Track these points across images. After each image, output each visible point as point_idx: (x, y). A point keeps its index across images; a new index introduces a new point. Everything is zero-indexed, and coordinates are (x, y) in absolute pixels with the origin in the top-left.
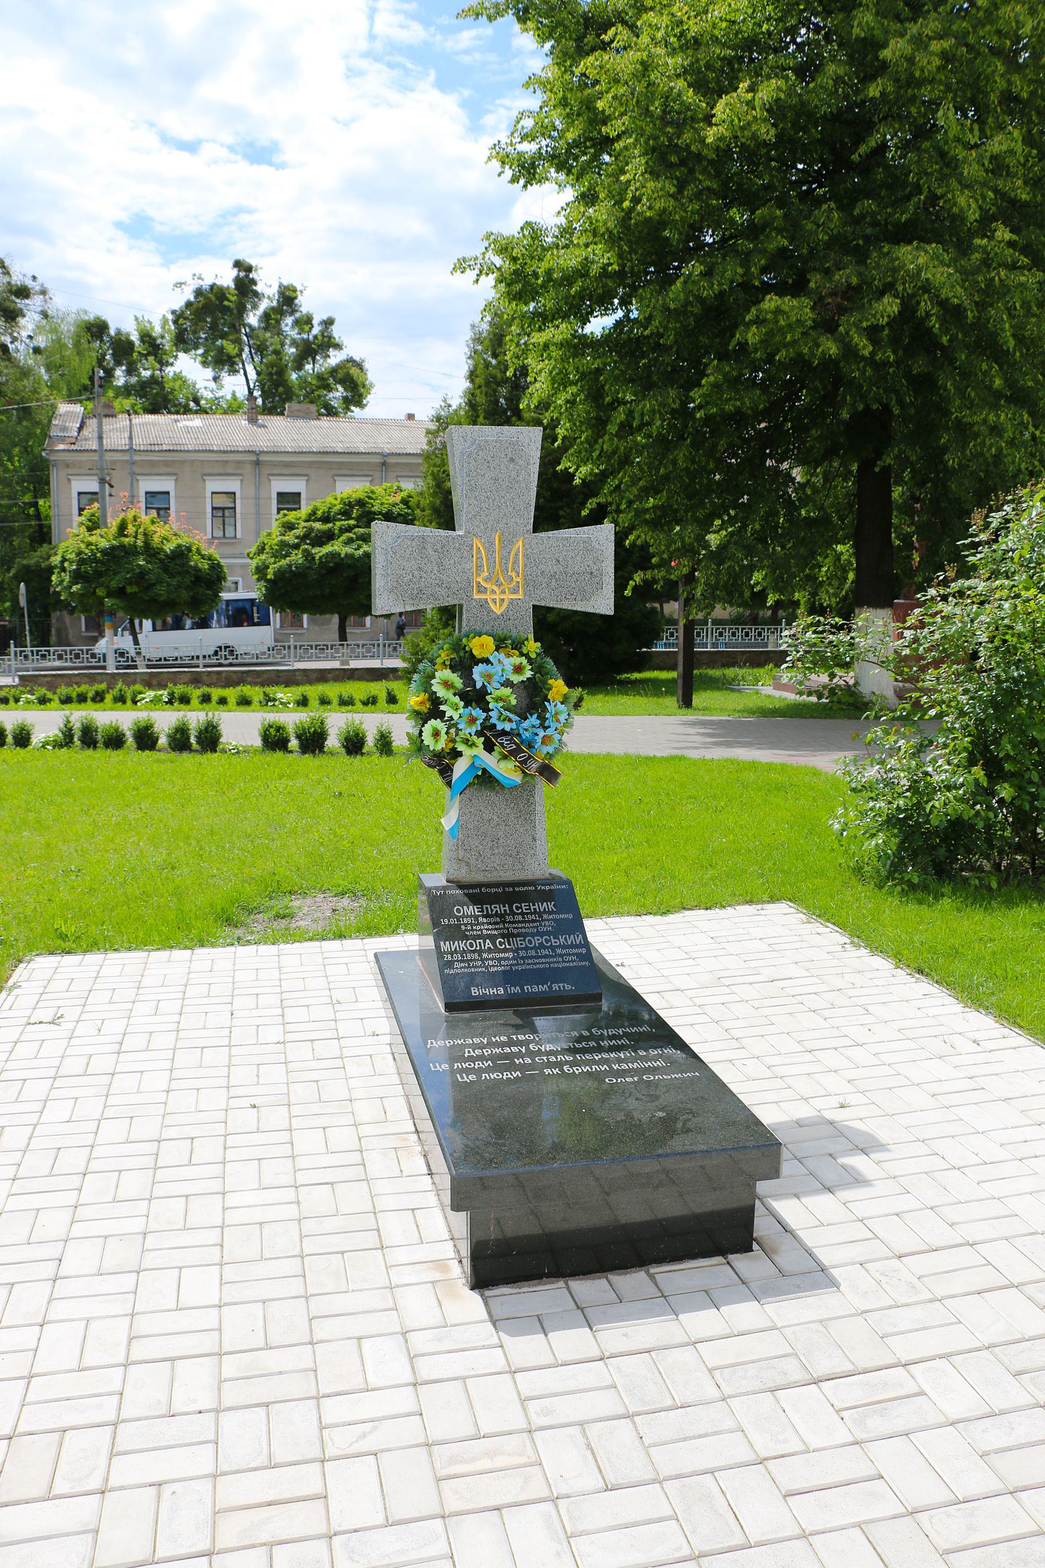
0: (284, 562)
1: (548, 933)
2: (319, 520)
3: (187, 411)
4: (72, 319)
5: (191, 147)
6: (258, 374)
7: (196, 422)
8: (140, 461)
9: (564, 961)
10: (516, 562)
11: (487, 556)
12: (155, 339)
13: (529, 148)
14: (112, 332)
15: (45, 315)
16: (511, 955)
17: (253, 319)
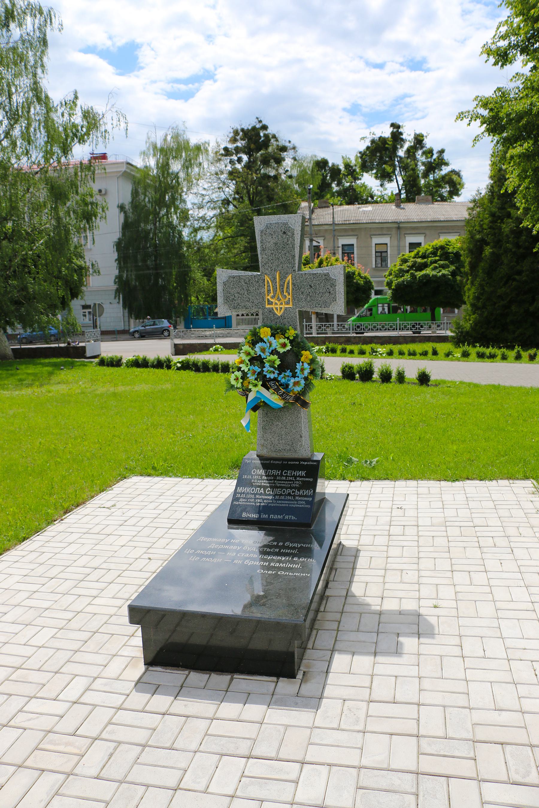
0: (401, 280)
1: (295, 488)
2: (420, 257)
3: (366, 202)
4: (309, 160)
5: (380, 66)
6: (404, 181)
7: (369, 208)
8: (336, 230)
9: (297, 504)
10: (288, 287)
11: (272, 285)
12: (352, 167)
13: (503, 44)
14: (330, 165)
15: (294, 159)
16: (270, 497)
17: (401, 153)
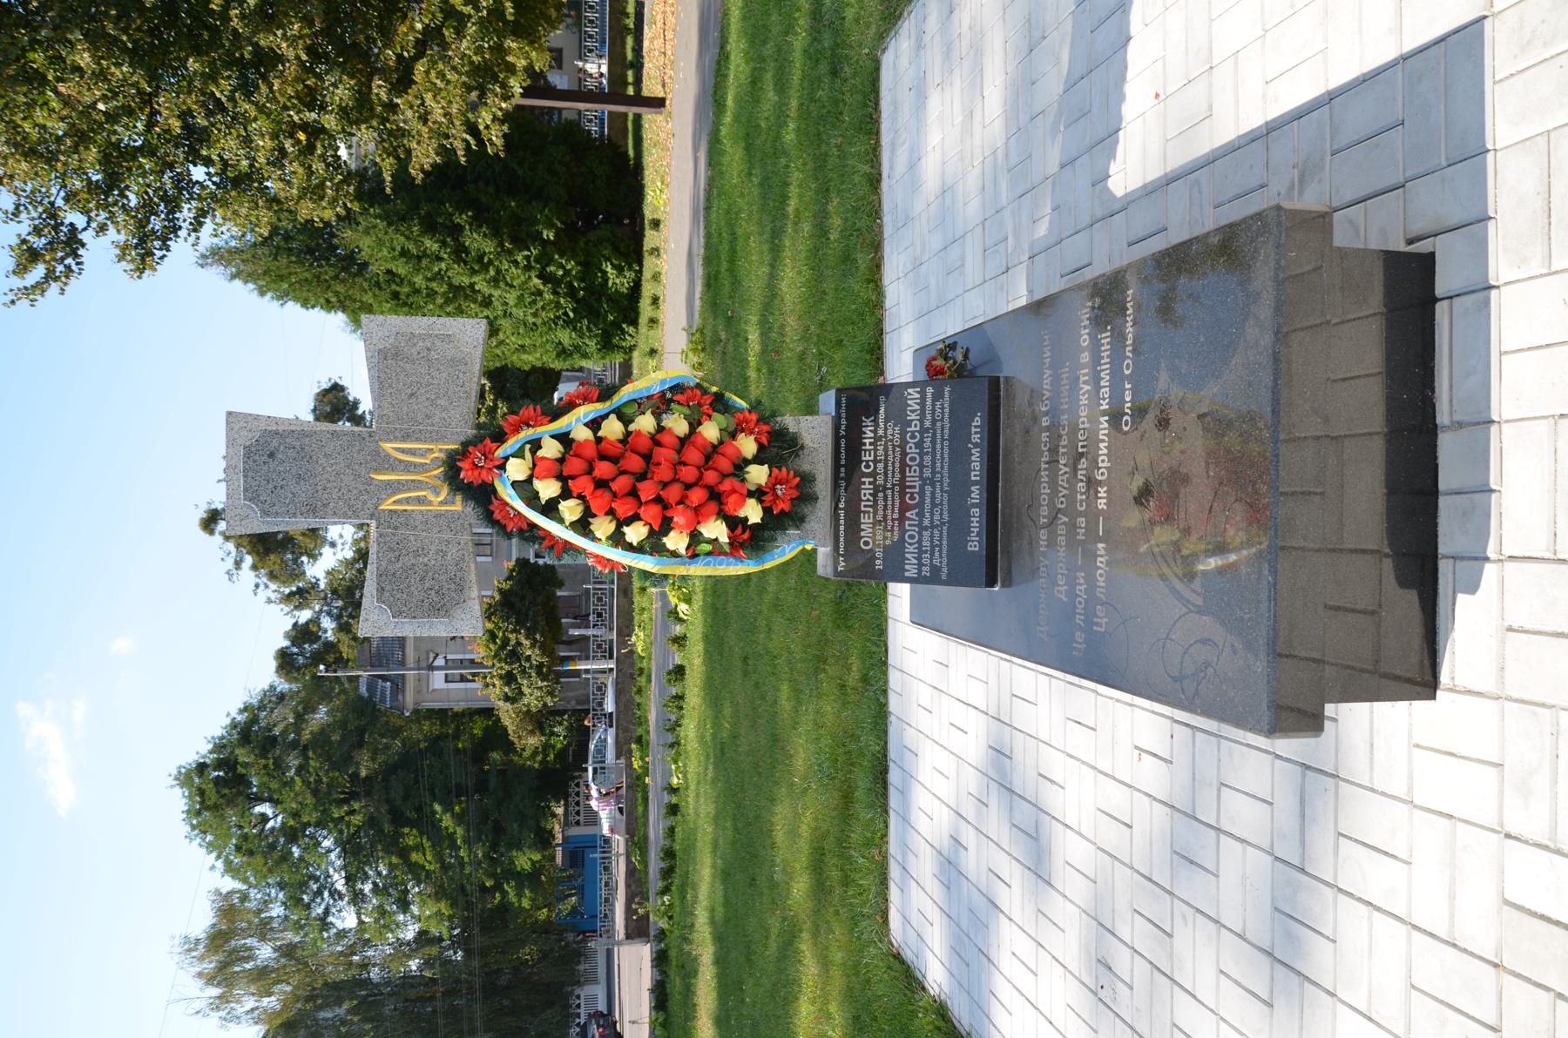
10: (412, 452)
14: (286, 643)
